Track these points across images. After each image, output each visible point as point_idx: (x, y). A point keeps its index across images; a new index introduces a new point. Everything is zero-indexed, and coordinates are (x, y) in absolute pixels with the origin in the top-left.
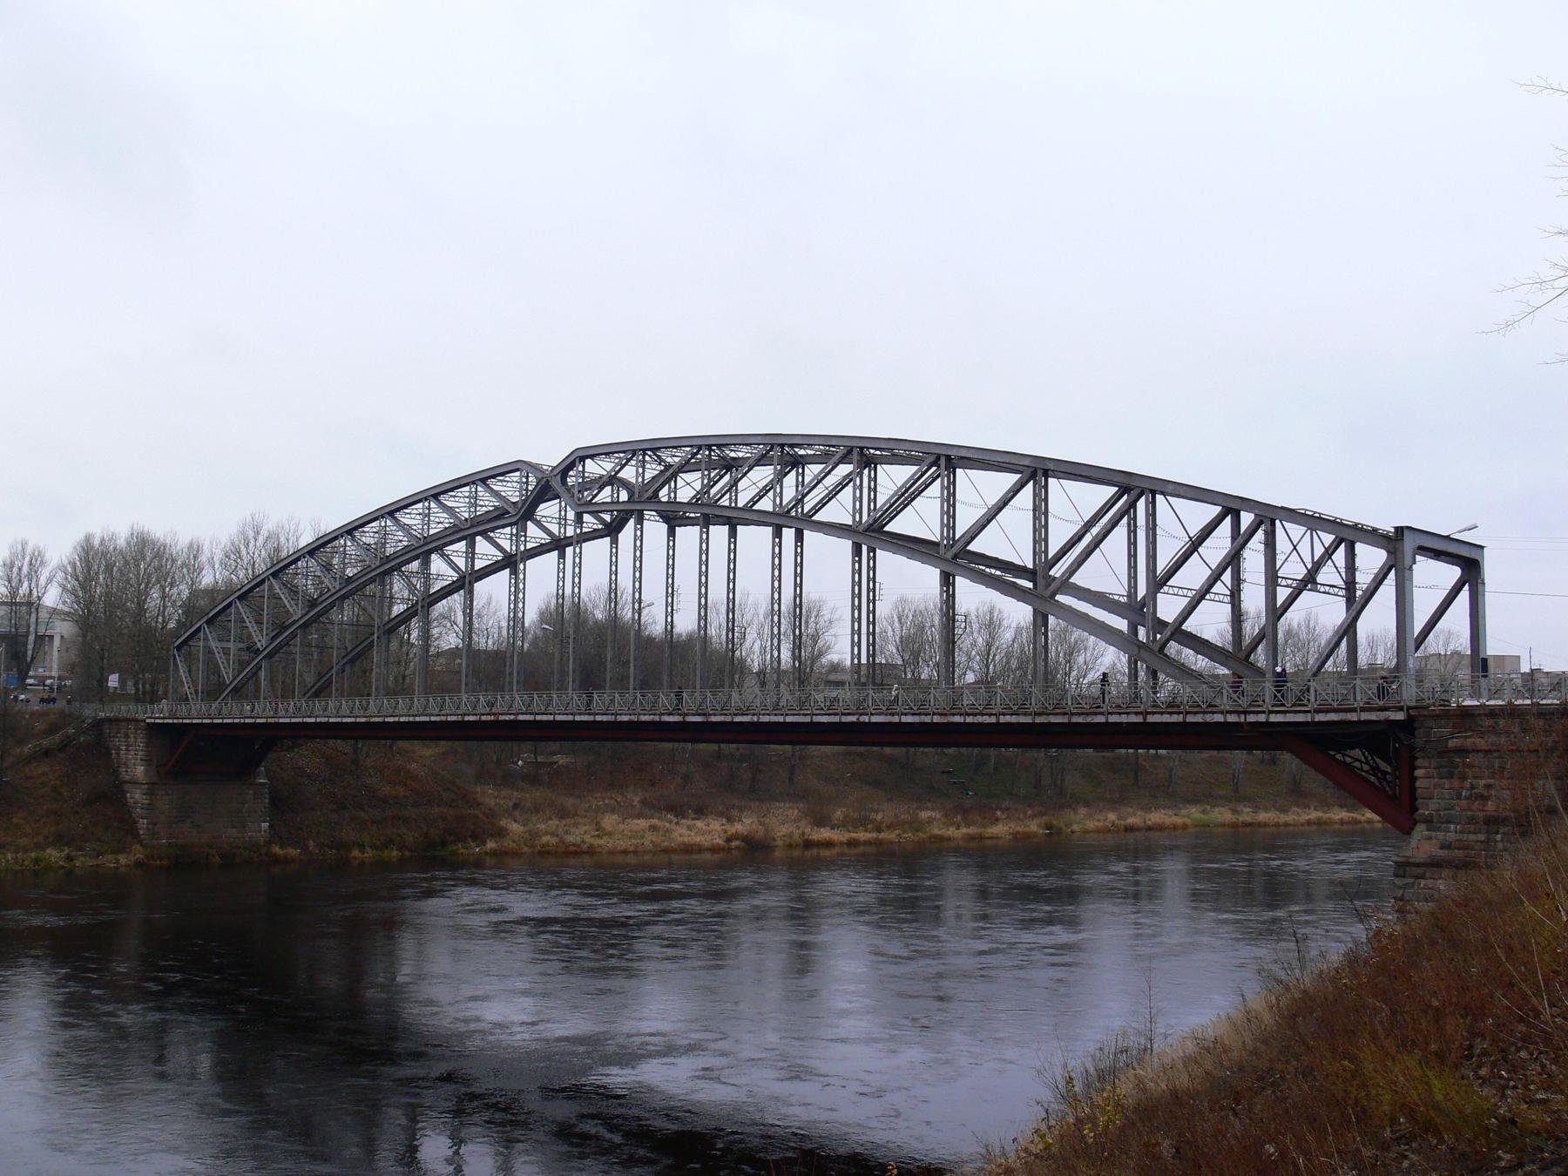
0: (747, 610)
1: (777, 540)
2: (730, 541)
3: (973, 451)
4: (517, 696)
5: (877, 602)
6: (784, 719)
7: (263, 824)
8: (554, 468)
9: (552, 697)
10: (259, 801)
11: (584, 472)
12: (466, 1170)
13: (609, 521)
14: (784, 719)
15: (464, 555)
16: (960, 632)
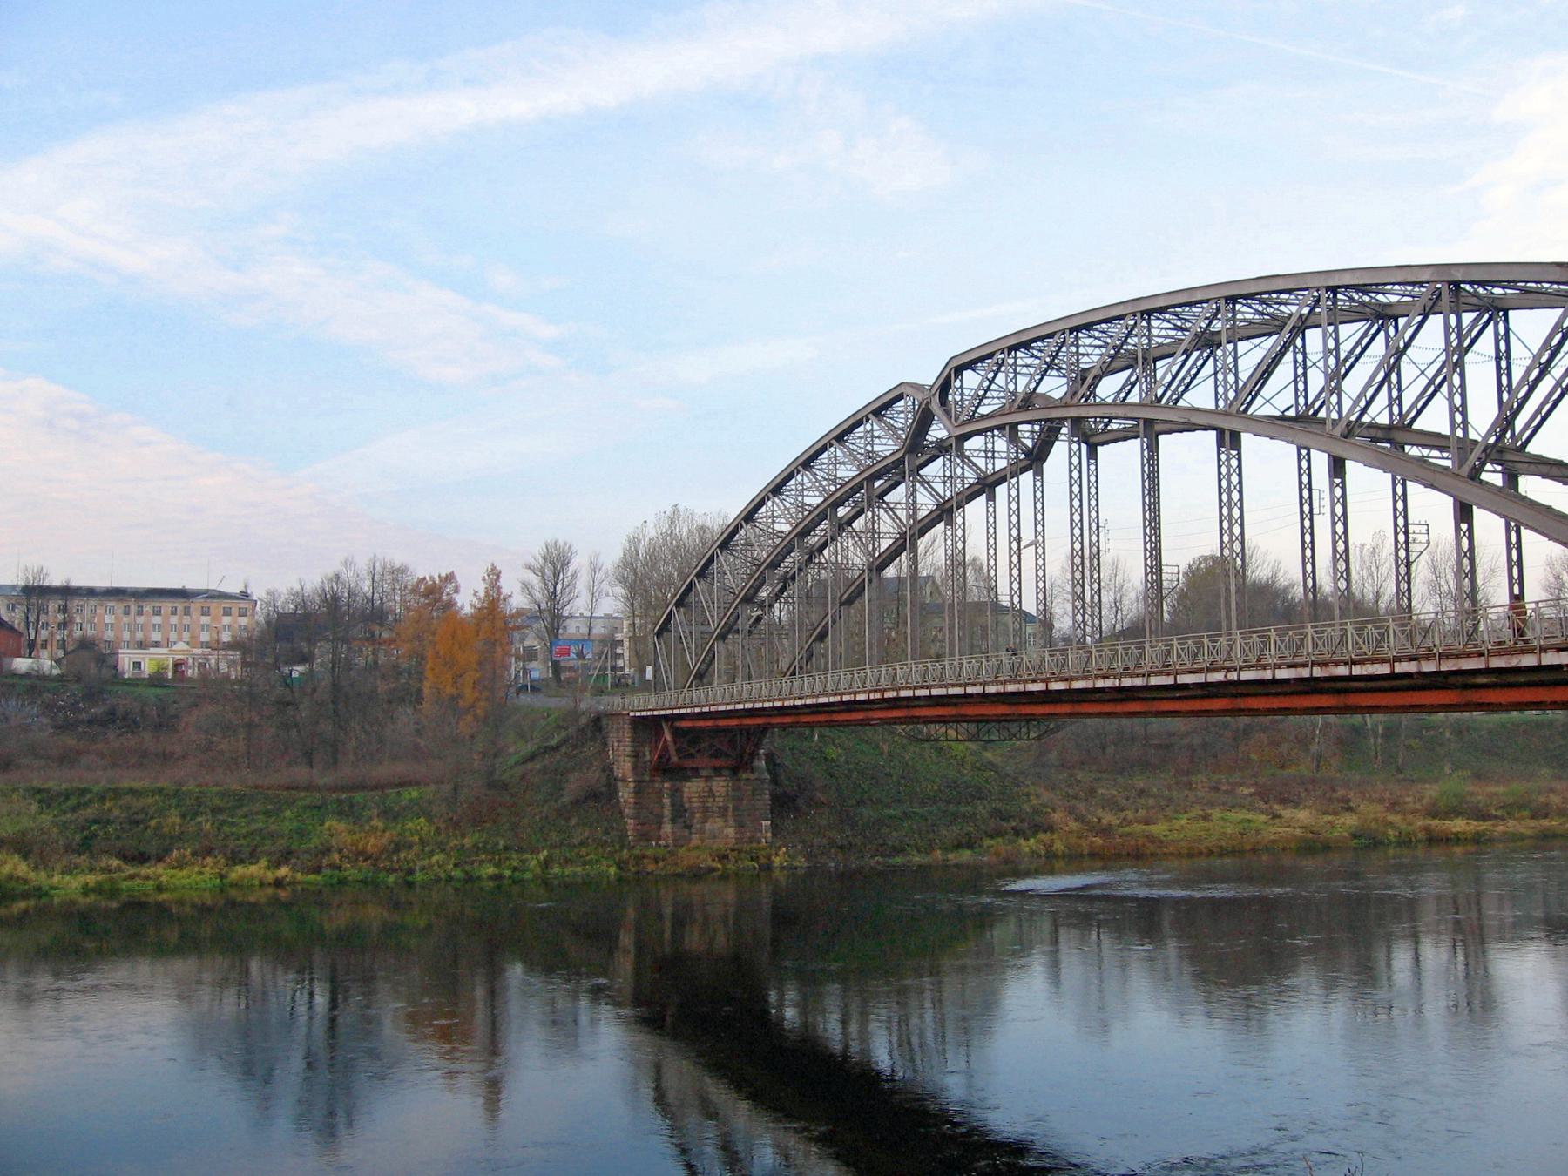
0: (1382, 562)
1: (1464, 526)
2: (1458, 529)
3: (1358, 274)
4: (1239, 636)
5: (1315, 517)
6: (1239, 676)
7: (764, 823)
8: (932, 386)
9: (1203, 643)
10: (759, 797)
11: (961, 387)
12: (1566, 700)
13: (1030, 446)
14: (1239, 676)
15: (918, 506)
16: (1420, 547)
